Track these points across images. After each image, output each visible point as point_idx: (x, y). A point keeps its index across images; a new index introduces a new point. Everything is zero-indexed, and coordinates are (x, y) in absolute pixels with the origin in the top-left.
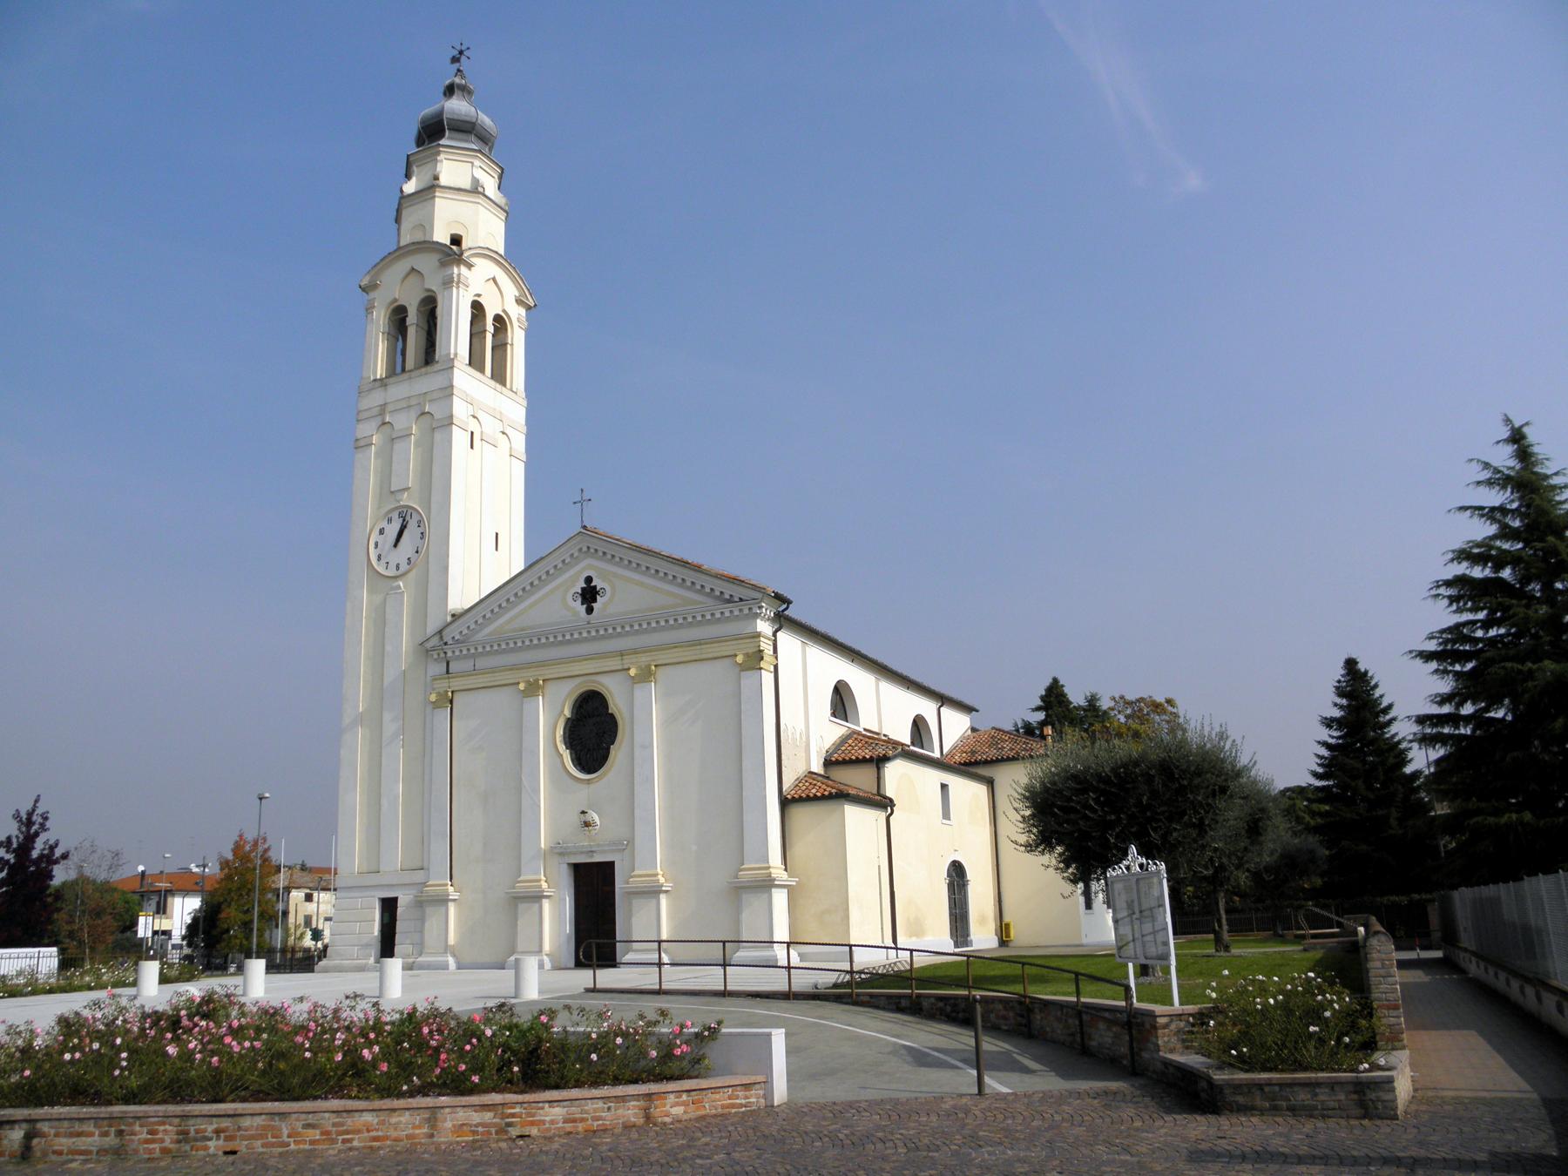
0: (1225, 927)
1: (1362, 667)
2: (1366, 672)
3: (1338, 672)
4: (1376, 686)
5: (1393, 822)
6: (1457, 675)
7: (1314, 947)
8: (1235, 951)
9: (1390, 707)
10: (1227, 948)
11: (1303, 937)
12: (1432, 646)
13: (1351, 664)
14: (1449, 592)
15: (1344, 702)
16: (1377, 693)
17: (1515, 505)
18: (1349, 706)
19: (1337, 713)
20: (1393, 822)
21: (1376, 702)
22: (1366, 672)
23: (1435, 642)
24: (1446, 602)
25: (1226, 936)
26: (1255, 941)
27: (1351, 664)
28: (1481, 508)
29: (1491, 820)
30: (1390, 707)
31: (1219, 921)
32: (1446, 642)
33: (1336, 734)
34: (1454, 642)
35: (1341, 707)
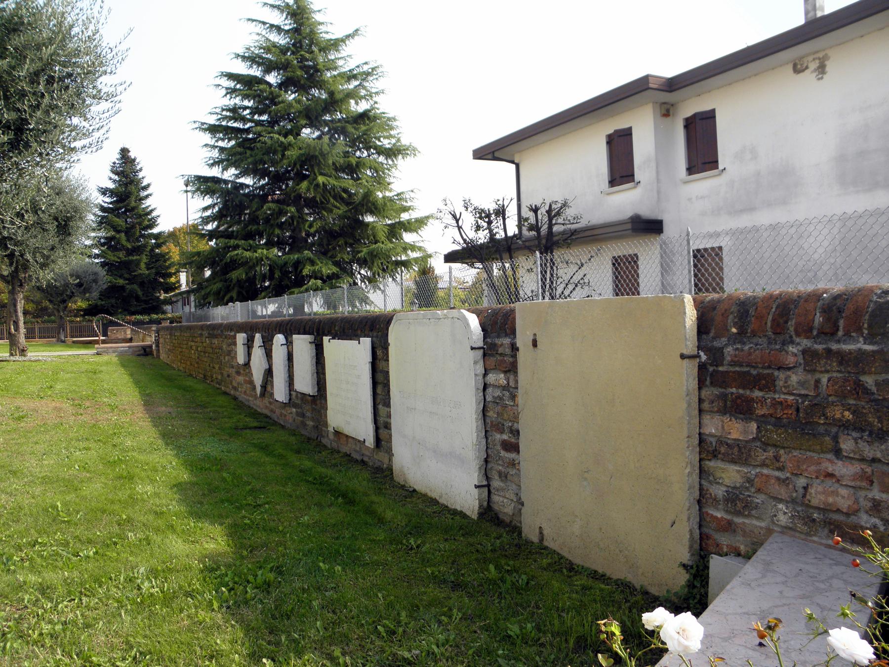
0: (22, 330)
1: (132, 155)
2: (134, 160)
3: (115, 156)
4: (141, 170)
5: (143, 266)
6: (222, 150)
7: (106, 351)
8: (31, 354)
9: (148, 185)
10: (23, 352)
11: (97, 342)
12: (212, 120)
13: (124, 152)
14: (231, 84)
15: (116, 178)
16: (141, 175)
17: (287, 28)
18: (120, 180)
19: (111, 186)
20: (143, 266)
21: (139, 181)
22: (134, 160)
23: (215, 117)
24: (224, 92)
25: (22, 339)
26: (42, 345)
27: (124, 152)
28: (264, 23)
29: (248, 254)
30: (148, 185)
31: (16, 323)
32: (225, 118)
33: (108, 200)
34: (230, 118)
35: (114, 181)
